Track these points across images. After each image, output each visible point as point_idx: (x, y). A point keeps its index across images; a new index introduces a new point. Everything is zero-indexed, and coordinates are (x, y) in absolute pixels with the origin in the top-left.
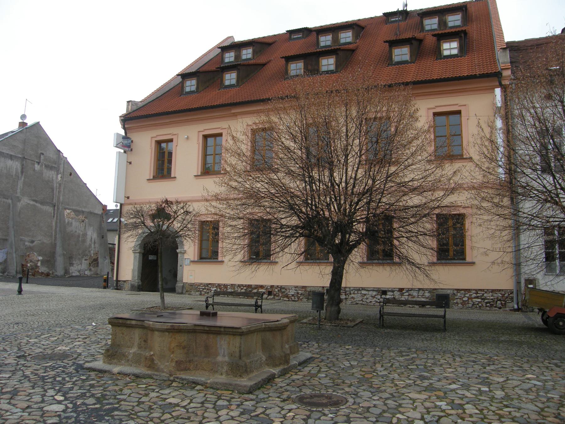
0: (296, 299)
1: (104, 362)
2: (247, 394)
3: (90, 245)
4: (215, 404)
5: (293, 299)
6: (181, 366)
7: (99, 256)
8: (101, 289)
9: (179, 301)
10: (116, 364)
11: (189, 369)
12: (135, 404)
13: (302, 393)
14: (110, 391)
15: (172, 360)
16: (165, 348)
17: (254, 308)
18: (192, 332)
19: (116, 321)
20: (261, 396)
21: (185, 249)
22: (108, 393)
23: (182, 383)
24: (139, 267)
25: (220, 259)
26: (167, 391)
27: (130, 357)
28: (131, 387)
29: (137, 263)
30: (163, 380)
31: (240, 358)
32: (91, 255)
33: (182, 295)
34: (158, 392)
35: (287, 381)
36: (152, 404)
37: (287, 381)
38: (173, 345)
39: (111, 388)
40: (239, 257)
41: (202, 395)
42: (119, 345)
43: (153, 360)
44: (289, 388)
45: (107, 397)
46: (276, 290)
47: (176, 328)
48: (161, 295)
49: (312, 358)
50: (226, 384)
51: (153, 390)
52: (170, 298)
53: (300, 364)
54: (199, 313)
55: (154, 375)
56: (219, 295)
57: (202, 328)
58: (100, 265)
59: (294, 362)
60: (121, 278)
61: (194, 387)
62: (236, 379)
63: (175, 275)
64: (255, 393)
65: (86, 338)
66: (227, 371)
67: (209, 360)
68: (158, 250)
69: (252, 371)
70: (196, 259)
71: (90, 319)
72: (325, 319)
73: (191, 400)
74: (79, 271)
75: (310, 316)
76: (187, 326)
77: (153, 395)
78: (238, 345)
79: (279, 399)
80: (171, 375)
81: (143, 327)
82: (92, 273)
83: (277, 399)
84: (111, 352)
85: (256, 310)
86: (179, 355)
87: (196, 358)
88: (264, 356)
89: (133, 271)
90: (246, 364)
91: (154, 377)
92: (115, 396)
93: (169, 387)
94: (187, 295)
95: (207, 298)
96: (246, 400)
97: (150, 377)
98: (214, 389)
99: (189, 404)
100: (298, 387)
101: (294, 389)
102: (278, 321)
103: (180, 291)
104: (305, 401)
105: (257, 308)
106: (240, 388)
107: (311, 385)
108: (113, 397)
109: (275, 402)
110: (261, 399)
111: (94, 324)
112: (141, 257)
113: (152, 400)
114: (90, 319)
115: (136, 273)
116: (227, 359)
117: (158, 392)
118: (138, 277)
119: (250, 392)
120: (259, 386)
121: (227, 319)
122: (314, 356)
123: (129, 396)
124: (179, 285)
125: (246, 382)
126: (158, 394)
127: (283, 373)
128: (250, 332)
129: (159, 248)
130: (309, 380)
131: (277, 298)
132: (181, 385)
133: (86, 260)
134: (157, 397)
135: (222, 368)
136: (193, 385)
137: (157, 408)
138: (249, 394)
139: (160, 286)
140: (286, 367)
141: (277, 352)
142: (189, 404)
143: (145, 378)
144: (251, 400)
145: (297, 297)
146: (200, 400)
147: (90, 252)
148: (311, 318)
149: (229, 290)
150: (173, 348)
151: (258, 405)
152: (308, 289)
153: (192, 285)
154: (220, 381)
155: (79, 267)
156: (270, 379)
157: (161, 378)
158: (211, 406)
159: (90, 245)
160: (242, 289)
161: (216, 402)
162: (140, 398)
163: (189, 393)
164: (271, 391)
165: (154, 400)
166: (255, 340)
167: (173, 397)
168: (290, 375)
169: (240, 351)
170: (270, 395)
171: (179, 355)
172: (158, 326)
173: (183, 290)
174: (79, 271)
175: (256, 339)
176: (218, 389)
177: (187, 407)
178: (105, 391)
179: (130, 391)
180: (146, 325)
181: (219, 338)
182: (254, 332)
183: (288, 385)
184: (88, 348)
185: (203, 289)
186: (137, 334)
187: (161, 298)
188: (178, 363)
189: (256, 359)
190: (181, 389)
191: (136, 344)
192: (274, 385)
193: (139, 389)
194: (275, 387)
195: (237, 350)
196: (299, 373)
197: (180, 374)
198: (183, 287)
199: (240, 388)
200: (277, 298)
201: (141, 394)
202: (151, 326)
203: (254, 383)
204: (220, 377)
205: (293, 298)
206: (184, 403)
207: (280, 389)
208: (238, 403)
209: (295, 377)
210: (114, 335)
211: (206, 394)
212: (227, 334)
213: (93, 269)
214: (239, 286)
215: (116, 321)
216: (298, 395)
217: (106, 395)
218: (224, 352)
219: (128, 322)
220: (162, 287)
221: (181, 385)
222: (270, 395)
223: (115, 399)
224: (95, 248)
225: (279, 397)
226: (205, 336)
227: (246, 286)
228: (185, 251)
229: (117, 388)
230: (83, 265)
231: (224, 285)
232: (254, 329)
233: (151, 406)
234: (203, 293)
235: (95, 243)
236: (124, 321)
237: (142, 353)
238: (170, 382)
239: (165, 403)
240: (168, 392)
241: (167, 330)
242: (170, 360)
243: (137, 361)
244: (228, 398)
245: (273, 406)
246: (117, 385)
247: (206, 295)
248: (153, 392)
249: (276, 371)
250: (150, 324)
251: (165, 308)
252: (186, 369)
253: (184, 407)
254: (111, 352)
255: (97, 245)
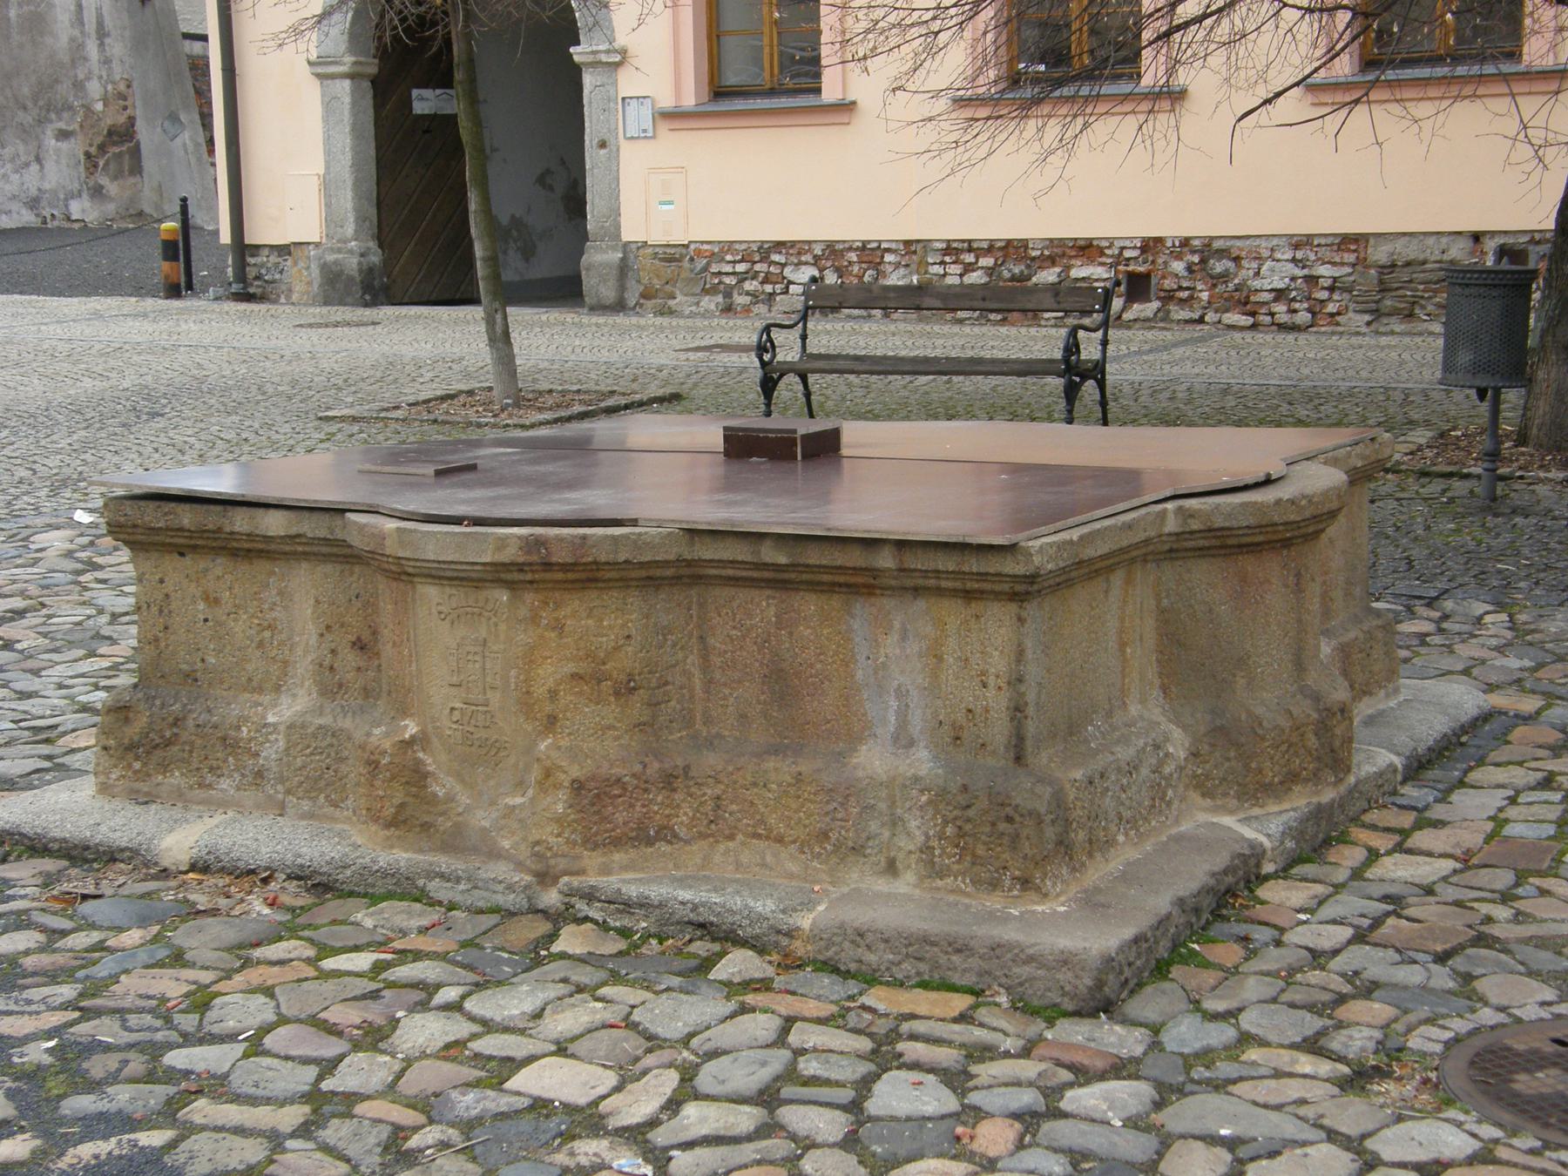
0: (1303, 317)
1: (104, 789)
2: (1078, 1014)
3: (77, 48)
4: (854, 1107)
5: (1283, 318)
6: (608, 811)
7: (139, 113)
8: (149, 303)
9: (605, 356)
10: (180, 798)
11: (666, 834)
12: (292, 1116)
13: (1487, 1016)
14: (120, 1012)
15: (548, 774)
16: (495, 698)
17: (1056, 383)
18: (676, 580)
19: (153, 516)
20: (1187, 1034)
21: (621, 40)
22: (106, 1030)
23: (624, 933)
24: (357, 166)
25: (831, 90)
26: (512, 1003)
27: (271, 753)
28: (271, 975)
29: (344, 140)
30: (495, 910)
31: (1018, 759)
32: (88, 109)
33: (620, 319)
34: (455, 1007)
35: (1350, 904)
36: (407, 1117)
37: (1350, 904)
38: (549, 673)
39: (131, 987)
40: (955, 62)
41: (761, 1026)
42: (190, 677)
43: (418, 777)
44: (1373, 962)
45: (97, 1066)
46: (1178, 267)
47: (561, 556)
48: (490, 321)
49: (1486, 717)
50: (926, 940)
51: (423, 996)
52: (549, 342)
53: (1417, 767)
54: (711, 435)
55: (431, 875)
56: (835, 309)
57: (740, 552)
58: (148, 163)
59: (1376, 758)
60: (257, 234)
61: (707, 964)
62: (994, 902)
63: (575, 204)
64: (1134, 1007)
65: (20, 614)
66: (926, 849)
67: (805, 767)
68: (448, 42)
69: (1099, 845)
70: (689, 101)
71: (64, 483)
72: (1522, 439)
73: (688, 1075)
74: (33, 204)
75: (1412, 423)
76: (637, 543)
77: (423, 1031)
78: (998, 664)
79: (1325, 1068)
80: (545, 878)
81: (341, 554)
82: (111, 208)
83: (1306, 1064)
84: (140, 723)
85: (1071, 393)
86: (597, 740)
87: (712, 760)
88: (1177, 733)
89: (328, 186)
90: (1058, 800)
91: (437, 889)
92: (154, 1051)
93: (538, 962)
94: (650, 319)
95: (767, 329)
96: (1083, 1075)
97: (407, 889)
98: (847, 975)
99: (673, 1105)
100: (1442, 958)
101: (1412, 975)
102: (1268, 481)
103: (608, 293)
104: (1524, 1083)
105: (1078, 382)
106: (1024, 971)
107: (1541, 943)
108: (137, 1064)
109: (1293, 1090)
110: (1188, 1061)
111: (82, 517)
112: (368, 102)
113: (409, 1085)
114: (64, 483)
115: (346, 201)
116: (922, 762)
117: (455, 1007)
118: (361, 219)
119: (1101, 1004)
120: (1158, 958)
121: (908, 474)
122: (1497, 700)
123: (256, 1048)
124: (598, 259)
125: (1067, 927)
126: (459, 1028)
127: (1314, 843)
128: (1083, 571)
129: (457, 29)
130: (1506, 898)
131: (1184, 314)
132: (614, 945)
133: (63, 135)
134: (452, 1050)
135: (895, 822)
136: (701, 948)
137: (444, 1145)
138: (1093, 1014)
139: (481, 270)
140: (1328, 795)
141: (1267, 700)
142: (673, 1105)
143: (374, 899)
144: (1120, 1069)
145: (1307, 305)
146: (746, 1074)
147: (79, 86)
148: (1421, 436)
149: (895, 279)
150: (553, 694)
151: (1177, 1117)
152: (1379, 254)
153: (672, 256)
154: (885, 917)
155: (31, 180)
156: (1231, 892)
157: (480, 899)
158: (826, 1124)
159: (77, 48)
160: (969, 267)
161: (865, 1085)
162: (329, 1066)
163: (674, 1013)
164: (1253, 988)
165: (422, 1078)
166: (1115, 629)
167: (562, 1049)
168: (1359, 855)
169: (1017, 710)
170: (1248, 1021)
171: (597, 740)
172: (436, 544)
173: (622, 288)
174: (33, 204)
175: (1120, 619)
176: (871, 979)
177: (659, 1137)
178: (88, 1014)
179: (259, 1010)
180: (356, 541)
181: (860, 617)
182: (1110, 569)
183: (1360, 937)
184: (25, 683)
185: (742, 278)
186: (303, 601)
187: (492, 341)
188: (593, 796)
189: (1124, 754)
190: (615, 978)
191: (303, 666)
192: (1261, 934)
193: (329, 986)
194: (1273, 959)
195: (997, 701)
196: (1421, 839)
197: (606, 870)
198: (624, 268)
199: (1024, 971)
200: (1184, 314)
201: (333, 1030)
202: (391, 548)
203: (1128, 933)
204: (882, 885)
205: (1280, 308)
206: (637, 1106)
207: (1315, 976)
208: (1027, 1098)
209: (1398, 870)
210: (154, 609)
211: (789, 1022)
212: (917, 591)
213: (112, 188)
214: (951, 249)
215: (153, 516)
216: (1460, 1026)
217: (95, 1047)
218: (903, 723)
219: (240, 522)
220: (495, 277)
221: (614, 945)
222: (1248, 1021)
223: (150, 1078)
224: (107, 61)
225: (1313, 1046)
226: (764, 607)
227: (991, 248)
228: (623, 52)
229: (171, 985)
230: (50, 165)
231: (864, 247)
232: (1103, 549)
233: (400, 1132)
234: (740, 300)
235: (102, 34)
236: (212, 518)
237: (347, 723)
238: (544, 927)
239: (503, 1103)
240: (529, 1006)
241: (502, 575)
242: (535, 774)
243: (317, 776)
244: (946, 1056)
245: (1287, 1127)
246: (178, 959)
247: (761, 309)
248: (423, 1006)
249: (1262, 827)
250: (383, 537)
251: (520, 400)
252: (646, 836)
253: (636, 1135)
254: (140, 723)
255: (117, 48)
